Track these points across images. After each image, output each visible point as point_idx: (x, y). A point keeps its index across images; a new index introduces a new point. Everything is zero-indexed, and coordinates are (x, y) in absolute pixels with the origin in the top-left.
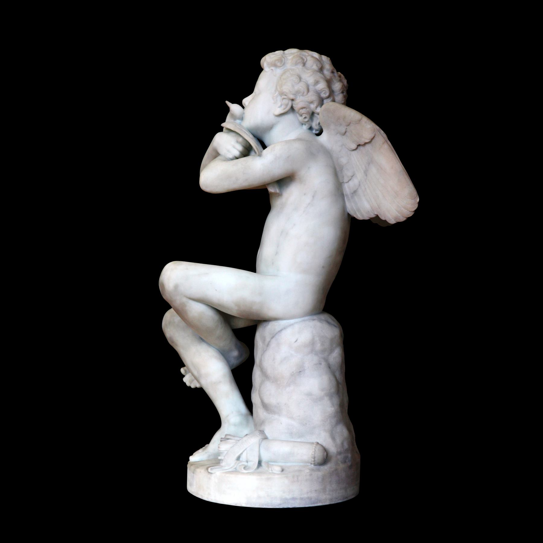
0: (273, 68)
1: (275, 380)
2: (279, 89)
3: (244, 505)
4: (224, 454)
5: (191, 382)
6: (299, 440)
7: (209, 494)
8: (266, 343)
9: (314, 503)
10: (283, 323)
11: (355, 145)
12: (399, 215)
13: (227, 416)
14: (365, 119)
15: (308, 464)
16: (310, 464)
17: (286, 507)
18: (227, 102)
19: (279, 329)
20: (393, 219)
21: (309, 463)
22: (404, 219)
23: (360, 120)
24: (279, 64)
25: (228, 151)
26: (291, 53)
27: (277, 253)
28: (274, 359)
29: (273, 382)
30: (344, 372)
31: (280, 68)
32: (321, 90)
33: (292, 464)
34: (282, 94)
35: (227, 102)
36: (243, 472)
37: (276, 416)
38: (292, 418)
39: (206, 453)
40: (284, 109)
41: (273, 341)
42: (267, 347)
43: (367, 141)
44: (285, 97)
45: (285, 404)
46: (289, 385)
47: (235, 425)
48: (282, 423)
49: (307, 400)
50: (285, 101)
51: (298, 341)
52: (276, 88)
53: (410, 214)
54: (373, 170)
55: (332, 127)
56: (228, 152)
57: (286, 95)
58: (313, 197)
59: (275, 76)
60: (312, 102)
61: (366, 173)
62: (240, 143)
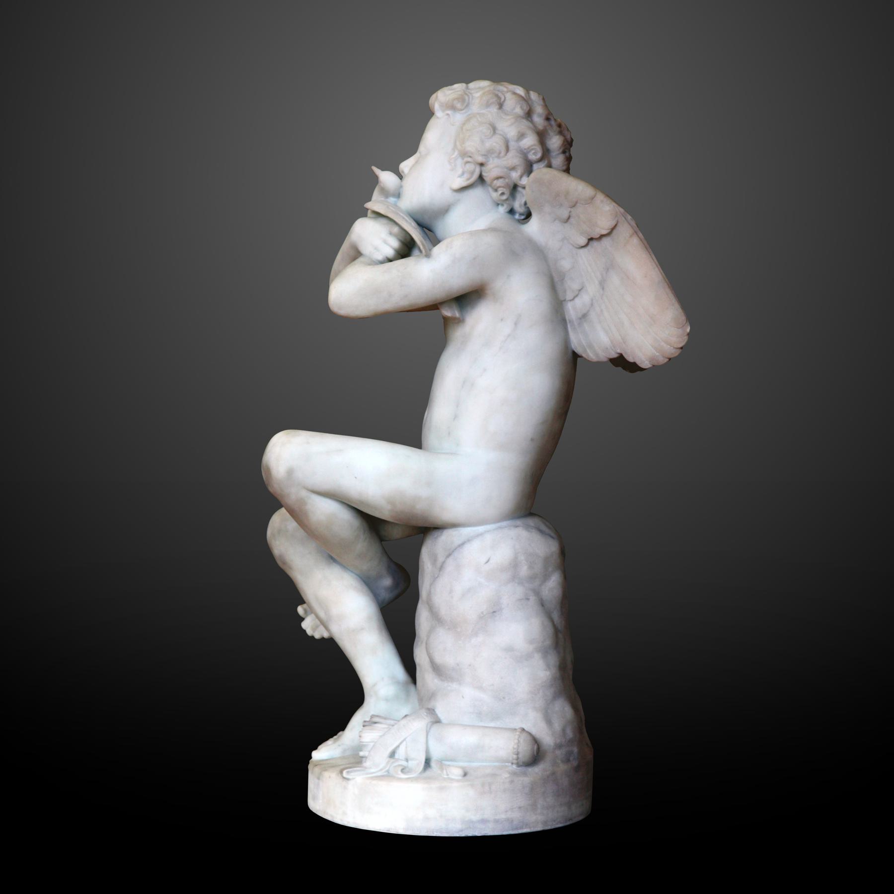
0: (449, 112)
1: (454, 626)
2: (459, 147)
3: (402, 832)
4: (369, 748)
5: (314, 629)
6: (492, 725)
7: (344, 813)
8: (439, 564)
9: (517, 829)
10: (466, 531)
11: (584, 238)
12: (658, 354)
13: (374, 685)
15: (507, 764)
16: (510, 764)
18: (375, 169)
19: (460, 542)
20: (647, 360)
21: (508, 763)
23: (592, 198)
24: (459, 105)
25: (376, 249)
26: (479, 88)
27: (456, 417)
28: (451, 592)
29: (449, 629)
31: (461, 112)
32: (528, 148)
33: (480, 764)
34: (464, 154)
35: (375, 169)
36: (400, 776)
37: (455, 686)
38: (480, 688)
39: (339, 746)
40: (468, 179)
41: (450, 561)
43: (604, 232)
44: (469, 159)
45: (470, 665)
46: (475, 634)
47: (387, 700)
48: (464, 696)
49: (506, 658)
50: (470, 167)
51: (491, 562)
52: (455, 146)
53: (673, 353)
54: (615, 280)
55: (547, 209)
56: (375, 251)
57: (470, 157)
58: (516, 324)
59: (453, 125)
60: (513, 169)
61: (602, 284)
62: (395, 235)
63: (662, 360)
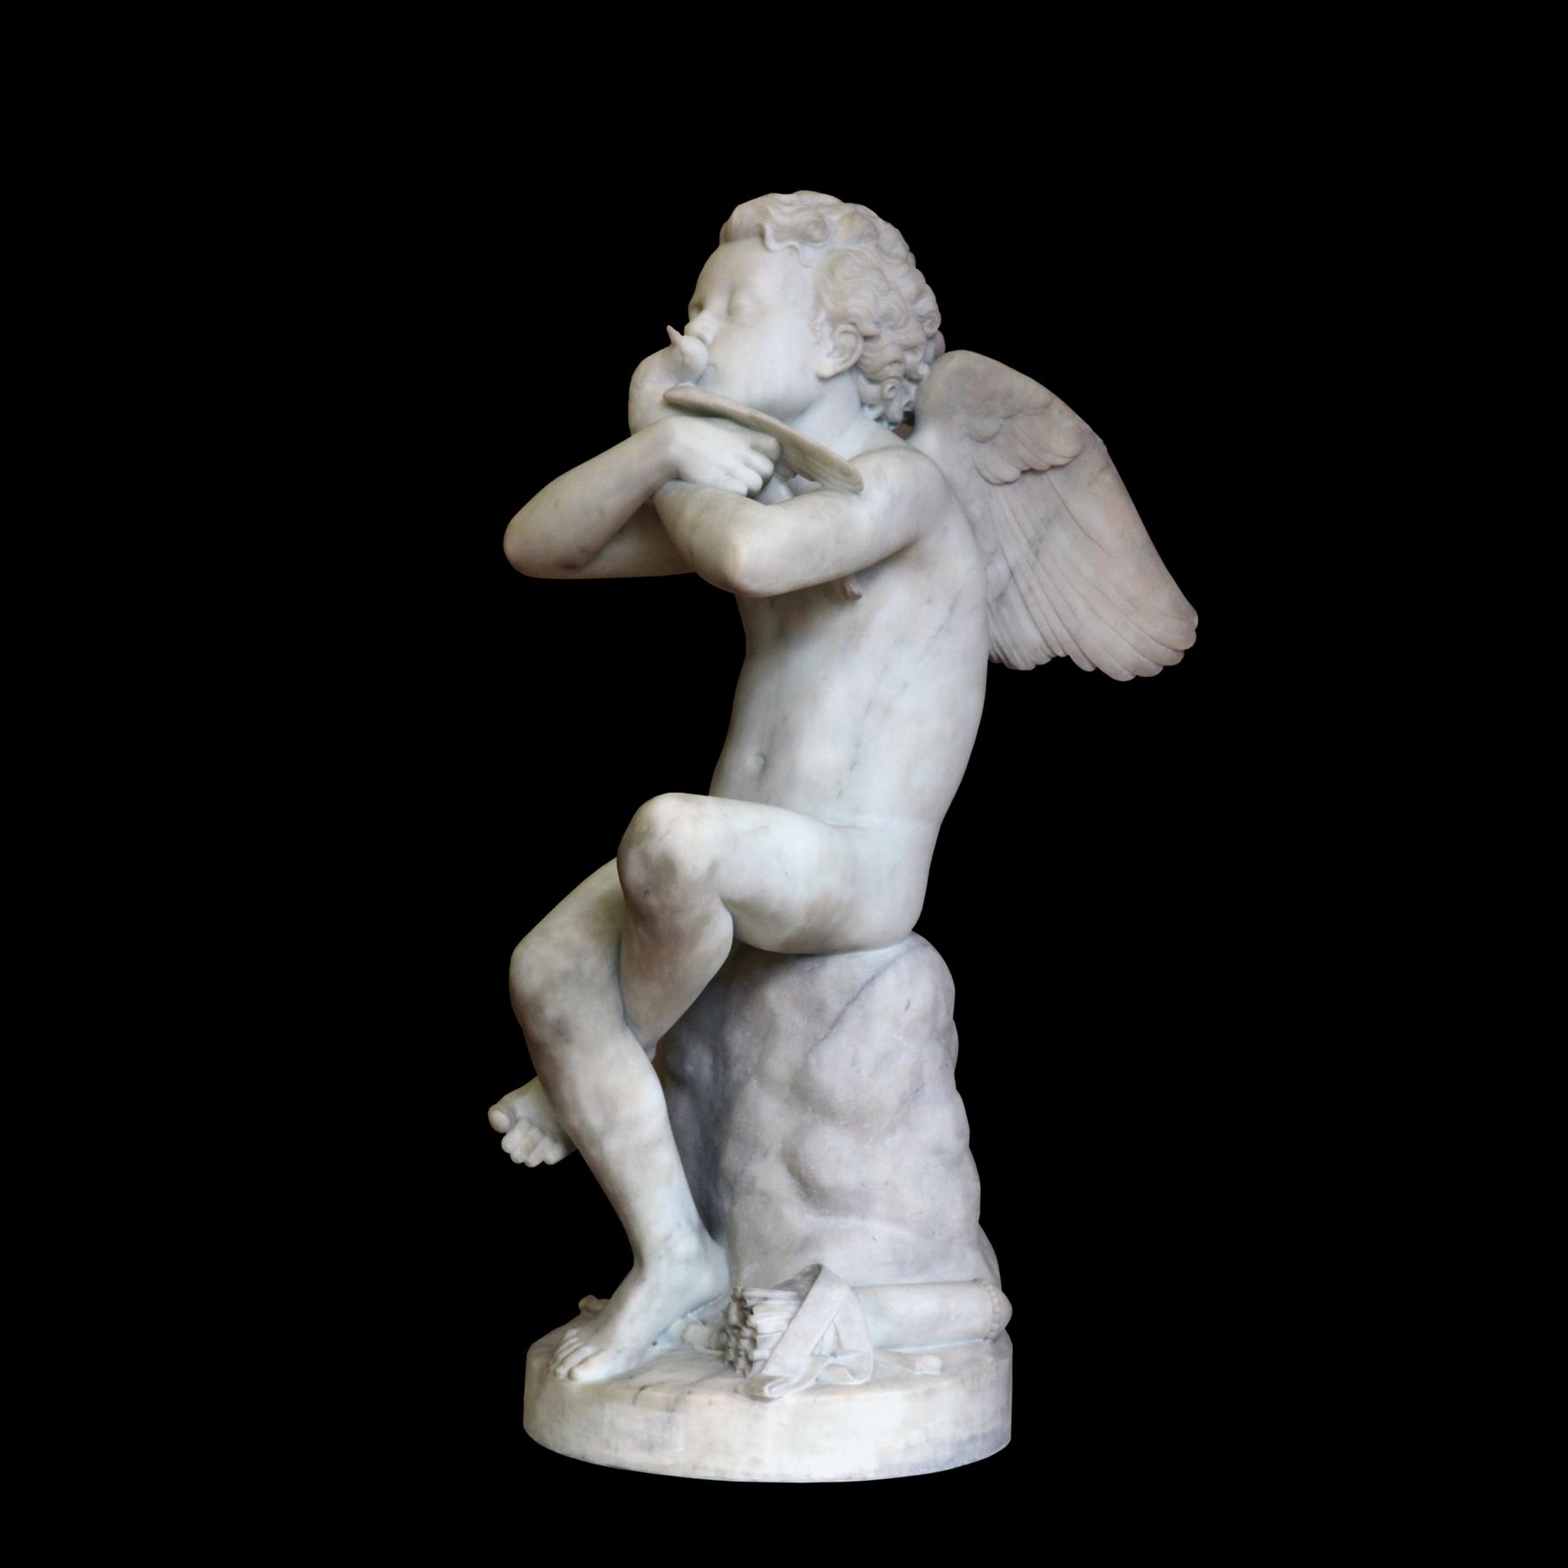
0: (796, 243)
1: (857, 1121)
2: (830, 305)
3: (871, 1476)
4: (771, 1344)
5: (529, 1151)
6: (918, 1279)
7: (755, 1461)
8: (830, 1016)
9: (998, 1446)
10: (872, 957)
11: (1015, 470)
12: (1145, 660)
13: (667, 1238)
14: (1059, 405)
15: (977, 1340)
16: (981, 1340)
17: (959, 1465)
18: (670, 329)
19: (868, 977)
20: (1126, 669)
21: (979, 1338)
22: (1031, 667)
23: (1047, 406)
24: (816, 234)
25: (730, 474)
26: (809, 207)
27: (854, 764)
28: (855, 1061)
29: (846, 1125)
30: (495, 1106)
31: (816, 245)
32: (925, 316)
33: (943, 1345)
34: (836, 320)
35: (670, 329)
36: (850, 1383)
37: (853, 1221)
38: (899, 1221)
39: (619, 1352)
40: (845, 362)
41: (854, 1010)
42: (832, 1028)
43: (1060, 461)
44: (850, 328)
45: (887, 1183)
46: (892, 1130)
47: (687, 1261)
48: (876, 1237)
49: (936, 1166)
50: (848, 341)
51: (913, 1006)
52: (819, 300)
53: (1175, 659)
54: (1061, 540)
55: (961, 417)
56: (727, 477)
57: (853, 324)
58: (952, 608)
59: (807, 267)
60: (911, 348)
61: (1036, 546)
62: (766, 453)
63: (1154, 670)
